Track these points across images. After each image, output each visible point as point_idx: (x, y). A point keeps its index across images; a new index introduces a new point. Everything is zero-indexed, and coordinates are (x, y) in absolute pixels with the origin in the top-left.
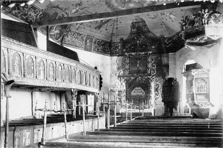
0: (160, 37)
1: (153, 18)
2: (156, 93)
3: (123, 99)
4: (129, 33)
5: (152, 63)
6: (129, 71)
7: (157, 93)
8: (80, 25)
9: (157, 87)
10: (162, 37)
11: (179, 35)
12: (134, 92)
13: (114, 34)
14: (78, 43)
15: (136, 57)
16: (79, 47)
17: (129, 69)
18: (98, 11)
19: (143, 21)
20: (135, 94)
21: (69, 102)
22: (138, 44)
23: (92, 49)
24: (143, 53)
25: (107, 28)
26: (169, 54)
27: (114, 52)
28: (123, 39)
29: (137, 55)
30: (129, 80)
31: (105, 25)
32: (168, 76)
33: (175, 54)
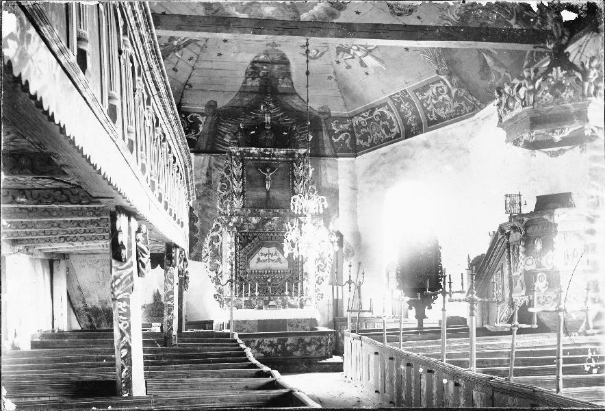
0: (319, 113)
4: (238, 88)
5: (307, 180)
10: (324, 113)
11: (377, 112)
12: (259, 259)
13: (191, 86)
15: (262, 160)
17: (243, 193)
19: (284, 62)
20: (261, 266)
21: (76, 288)
22: (268, 123)
24: (282, 152)
25: (179, 64)
29: (264, 155)
30: (243, 225)
31: (177, 54)
32: (337, 219)
33: (353, 162)
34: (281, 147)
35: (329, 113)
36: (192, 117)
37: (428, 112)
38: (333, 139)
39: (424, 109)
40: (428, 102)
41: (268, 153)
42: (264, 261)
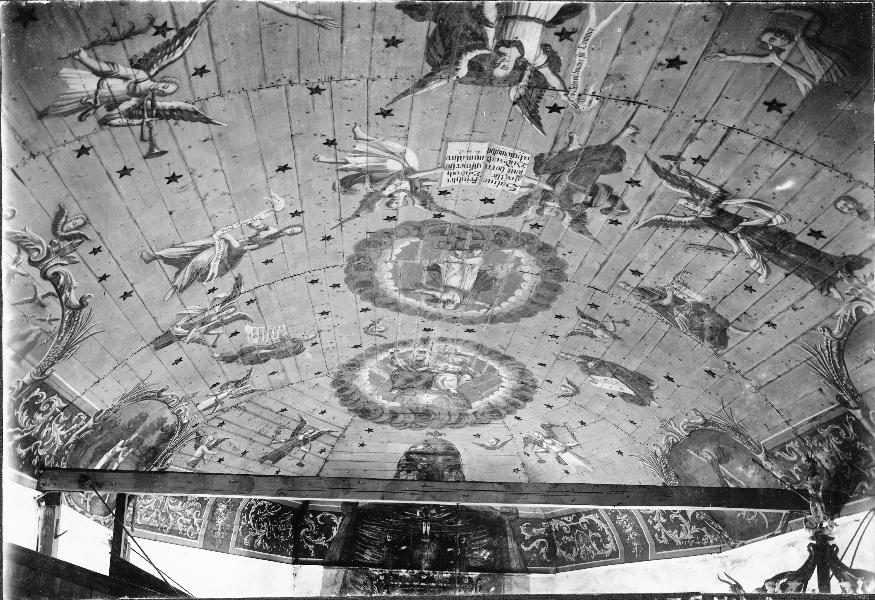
1: (488, 448)
8: (210, 449)
11: (583, 519)
14: (182, 518)
16: (182, 535)
18: (294, 403)
19: (452, 453)
23: (233, 538)
27: (311, 547)
31: (303, 448)
34: (442, 569)
35: (517, 513)
37: (656, 531)
38: (523, 547)
39: (650, 527)
40: (655, 519)
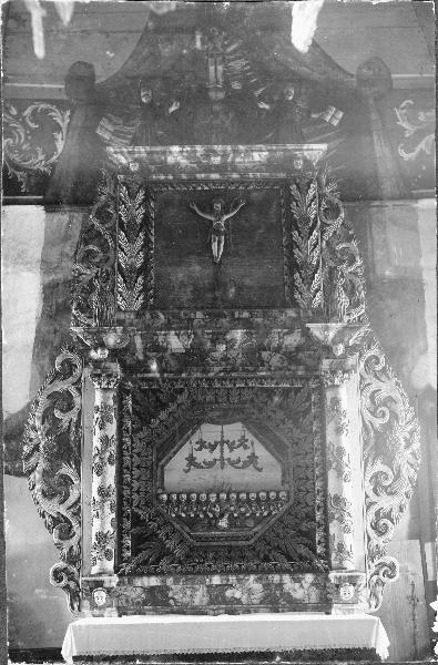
0: (362, 81)
2: (376, 476)
3: (97, 522)
5: (329, 233)
6: (145, 289)
7: (385, 468)
9: (378, 422)
12: (191, 460)
13: (388, 516)
15: (199, 182)
17: (144, 270)
20: (197, 479)
24: (256, 156)
26: (414, 209)
28: (92, 77)
36: (34, 113)
38: (402, 153)
41: (217, 160)
42: (210, 465)
